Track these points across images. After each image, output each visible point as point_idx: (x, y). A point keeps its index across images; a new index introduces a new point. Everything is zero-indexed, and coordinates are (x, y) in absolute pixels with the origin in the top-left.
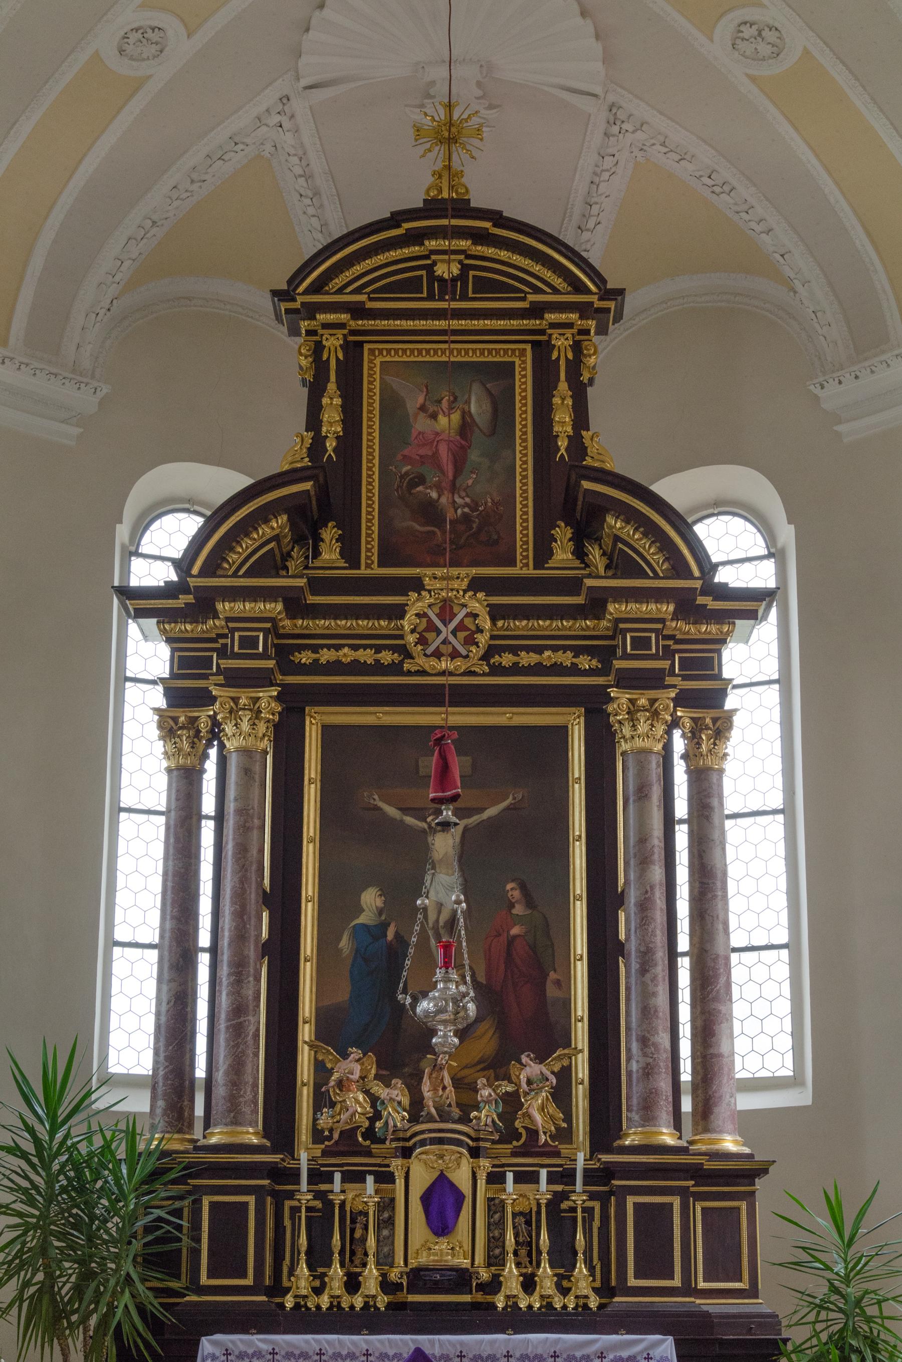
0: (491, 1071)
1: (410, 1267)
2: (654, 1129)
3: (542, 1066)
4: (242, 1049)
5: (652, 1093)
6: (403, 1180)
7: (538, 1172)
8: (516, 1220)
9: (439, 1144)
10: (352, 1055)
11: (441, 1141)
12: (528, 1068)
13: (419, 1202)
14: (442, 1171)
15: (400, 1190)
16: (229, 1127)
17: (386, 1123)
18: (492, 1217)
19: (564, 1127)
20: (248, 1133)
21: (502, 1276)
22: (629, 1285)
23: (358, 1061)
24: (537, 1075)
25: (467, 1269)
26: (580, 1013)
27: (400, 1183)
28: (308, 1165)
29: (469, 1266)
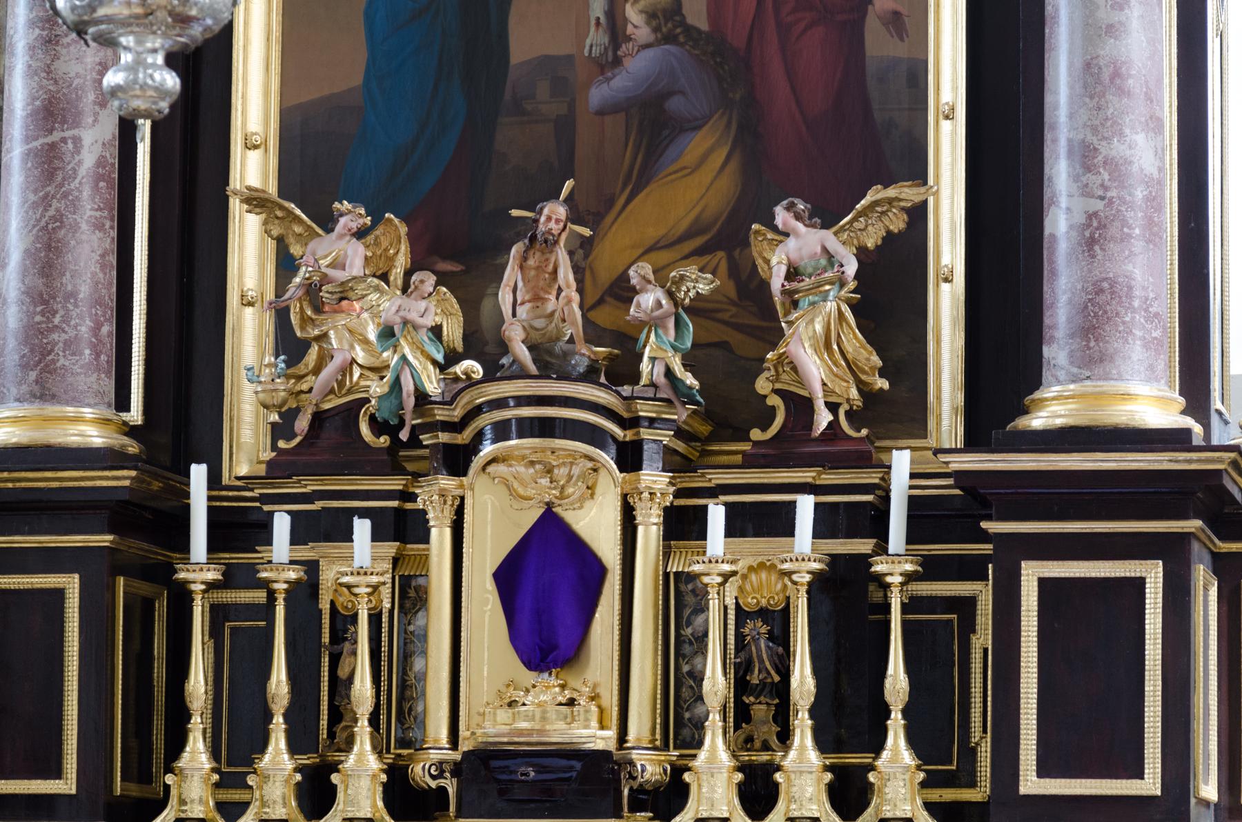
0: (721, 254)
1: (465, 746)
2: (1107, 386)
3: (828, 237)
4: (58, 210)
5: (1100, 291)
6: (448, 532)
7: (793, 504)
8: (747, 631)
9: (542, 435)
10: (342, 220)
11: (545, 428)
12: (791, 243)
13: (490, 585)
14: (548, 504)
15: (440, 555)
16: (26, 406)
17: (396, 384)
18: (689, 624)
19: (881, 389)
20: (77, 420)
21: (689, 769)
22: (1023, 790)
23: (360, 234)
24: (813, 256)
25: (605, 755)
26: (946, 96)
27: (441, 537)
28: (210, 498)
29: (611, 746)
